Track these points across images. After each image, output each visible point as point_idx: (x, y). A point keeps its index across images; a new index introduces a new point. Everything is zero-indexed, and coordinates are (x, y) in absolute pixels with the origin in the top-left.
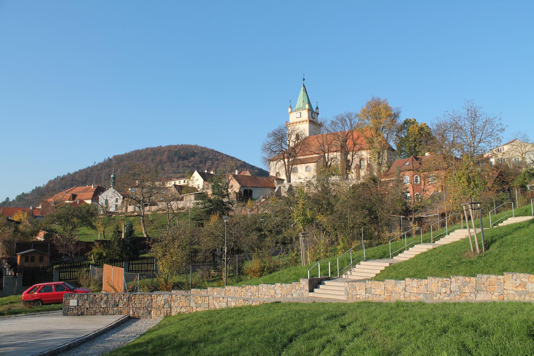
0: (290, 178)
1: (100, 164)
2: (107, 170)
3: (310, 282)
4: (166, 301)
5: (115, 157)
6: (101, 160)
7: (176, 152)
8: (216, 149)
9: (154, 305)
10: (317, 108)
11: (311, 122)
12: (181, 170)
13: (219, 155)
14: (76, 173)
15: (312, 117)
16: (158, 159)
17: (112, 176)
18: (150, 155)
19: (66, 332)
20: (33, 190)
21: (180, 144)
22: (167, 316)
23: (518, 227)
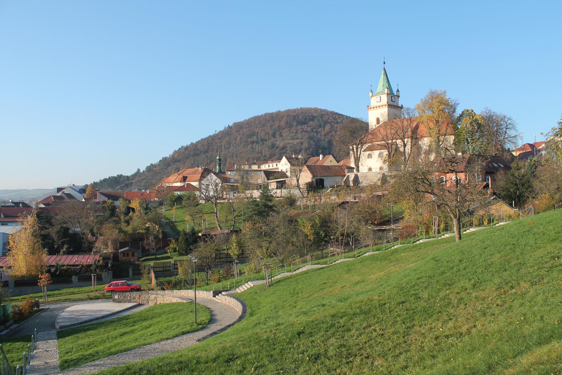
0: (358, 167)
1: (220, 132)
2: (228, 139)
3: (214, 292)
4: (155, 298)
5: (235, 124)
6: (222, 129)
7: (295, 116)
8: (336, 111)
10: (398, 91)
11: (389, 106)
12: (299, 135)
13: (339, 118)
14: (198, 142)
15: (392, 101)
16: (277, 125)
17: (218, 158)
18: (269, 121)
19: (108, 311)
20: (160, 161)
21: (299, 108)
22: (156, 304)
23: (474, 233)
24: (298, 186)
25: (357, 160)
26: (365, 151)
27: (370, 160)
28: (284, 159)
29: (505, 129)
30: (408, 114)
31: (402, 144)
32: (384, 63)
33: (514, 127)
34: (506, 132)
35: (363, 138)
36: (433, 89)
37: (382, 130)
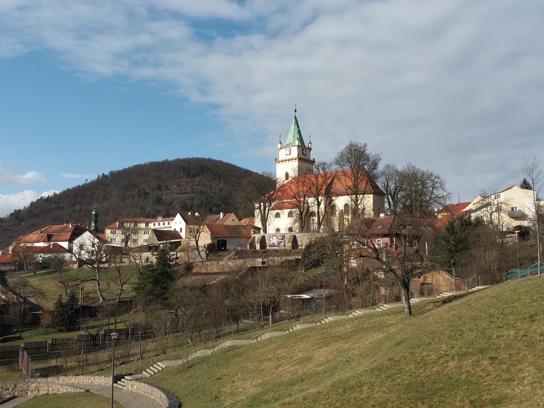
0: (266, 227)
4: (36, 387)
5: (112, 173)
9: (30, 389)
11: (300, 159)
15: (303, 154)
17: (93, 213)
24: (197, 248)
25: (264, 220)
26: (273, 209)
27: (277, 219)
28: (178, 217)
29: (431, 189)
30: (324, 169)
31: (316, 203)
32: (296, 111)
33: (442, 187)
34: (432, 192)
35: (272, 195)
36: (353, 141)
37: (293, 187)
